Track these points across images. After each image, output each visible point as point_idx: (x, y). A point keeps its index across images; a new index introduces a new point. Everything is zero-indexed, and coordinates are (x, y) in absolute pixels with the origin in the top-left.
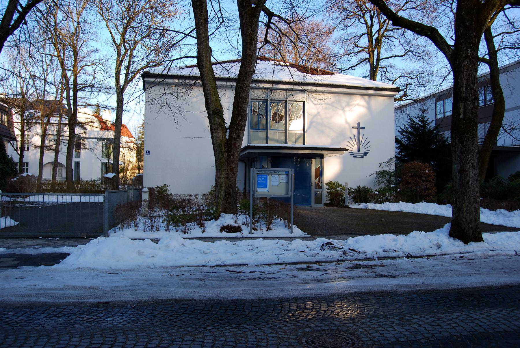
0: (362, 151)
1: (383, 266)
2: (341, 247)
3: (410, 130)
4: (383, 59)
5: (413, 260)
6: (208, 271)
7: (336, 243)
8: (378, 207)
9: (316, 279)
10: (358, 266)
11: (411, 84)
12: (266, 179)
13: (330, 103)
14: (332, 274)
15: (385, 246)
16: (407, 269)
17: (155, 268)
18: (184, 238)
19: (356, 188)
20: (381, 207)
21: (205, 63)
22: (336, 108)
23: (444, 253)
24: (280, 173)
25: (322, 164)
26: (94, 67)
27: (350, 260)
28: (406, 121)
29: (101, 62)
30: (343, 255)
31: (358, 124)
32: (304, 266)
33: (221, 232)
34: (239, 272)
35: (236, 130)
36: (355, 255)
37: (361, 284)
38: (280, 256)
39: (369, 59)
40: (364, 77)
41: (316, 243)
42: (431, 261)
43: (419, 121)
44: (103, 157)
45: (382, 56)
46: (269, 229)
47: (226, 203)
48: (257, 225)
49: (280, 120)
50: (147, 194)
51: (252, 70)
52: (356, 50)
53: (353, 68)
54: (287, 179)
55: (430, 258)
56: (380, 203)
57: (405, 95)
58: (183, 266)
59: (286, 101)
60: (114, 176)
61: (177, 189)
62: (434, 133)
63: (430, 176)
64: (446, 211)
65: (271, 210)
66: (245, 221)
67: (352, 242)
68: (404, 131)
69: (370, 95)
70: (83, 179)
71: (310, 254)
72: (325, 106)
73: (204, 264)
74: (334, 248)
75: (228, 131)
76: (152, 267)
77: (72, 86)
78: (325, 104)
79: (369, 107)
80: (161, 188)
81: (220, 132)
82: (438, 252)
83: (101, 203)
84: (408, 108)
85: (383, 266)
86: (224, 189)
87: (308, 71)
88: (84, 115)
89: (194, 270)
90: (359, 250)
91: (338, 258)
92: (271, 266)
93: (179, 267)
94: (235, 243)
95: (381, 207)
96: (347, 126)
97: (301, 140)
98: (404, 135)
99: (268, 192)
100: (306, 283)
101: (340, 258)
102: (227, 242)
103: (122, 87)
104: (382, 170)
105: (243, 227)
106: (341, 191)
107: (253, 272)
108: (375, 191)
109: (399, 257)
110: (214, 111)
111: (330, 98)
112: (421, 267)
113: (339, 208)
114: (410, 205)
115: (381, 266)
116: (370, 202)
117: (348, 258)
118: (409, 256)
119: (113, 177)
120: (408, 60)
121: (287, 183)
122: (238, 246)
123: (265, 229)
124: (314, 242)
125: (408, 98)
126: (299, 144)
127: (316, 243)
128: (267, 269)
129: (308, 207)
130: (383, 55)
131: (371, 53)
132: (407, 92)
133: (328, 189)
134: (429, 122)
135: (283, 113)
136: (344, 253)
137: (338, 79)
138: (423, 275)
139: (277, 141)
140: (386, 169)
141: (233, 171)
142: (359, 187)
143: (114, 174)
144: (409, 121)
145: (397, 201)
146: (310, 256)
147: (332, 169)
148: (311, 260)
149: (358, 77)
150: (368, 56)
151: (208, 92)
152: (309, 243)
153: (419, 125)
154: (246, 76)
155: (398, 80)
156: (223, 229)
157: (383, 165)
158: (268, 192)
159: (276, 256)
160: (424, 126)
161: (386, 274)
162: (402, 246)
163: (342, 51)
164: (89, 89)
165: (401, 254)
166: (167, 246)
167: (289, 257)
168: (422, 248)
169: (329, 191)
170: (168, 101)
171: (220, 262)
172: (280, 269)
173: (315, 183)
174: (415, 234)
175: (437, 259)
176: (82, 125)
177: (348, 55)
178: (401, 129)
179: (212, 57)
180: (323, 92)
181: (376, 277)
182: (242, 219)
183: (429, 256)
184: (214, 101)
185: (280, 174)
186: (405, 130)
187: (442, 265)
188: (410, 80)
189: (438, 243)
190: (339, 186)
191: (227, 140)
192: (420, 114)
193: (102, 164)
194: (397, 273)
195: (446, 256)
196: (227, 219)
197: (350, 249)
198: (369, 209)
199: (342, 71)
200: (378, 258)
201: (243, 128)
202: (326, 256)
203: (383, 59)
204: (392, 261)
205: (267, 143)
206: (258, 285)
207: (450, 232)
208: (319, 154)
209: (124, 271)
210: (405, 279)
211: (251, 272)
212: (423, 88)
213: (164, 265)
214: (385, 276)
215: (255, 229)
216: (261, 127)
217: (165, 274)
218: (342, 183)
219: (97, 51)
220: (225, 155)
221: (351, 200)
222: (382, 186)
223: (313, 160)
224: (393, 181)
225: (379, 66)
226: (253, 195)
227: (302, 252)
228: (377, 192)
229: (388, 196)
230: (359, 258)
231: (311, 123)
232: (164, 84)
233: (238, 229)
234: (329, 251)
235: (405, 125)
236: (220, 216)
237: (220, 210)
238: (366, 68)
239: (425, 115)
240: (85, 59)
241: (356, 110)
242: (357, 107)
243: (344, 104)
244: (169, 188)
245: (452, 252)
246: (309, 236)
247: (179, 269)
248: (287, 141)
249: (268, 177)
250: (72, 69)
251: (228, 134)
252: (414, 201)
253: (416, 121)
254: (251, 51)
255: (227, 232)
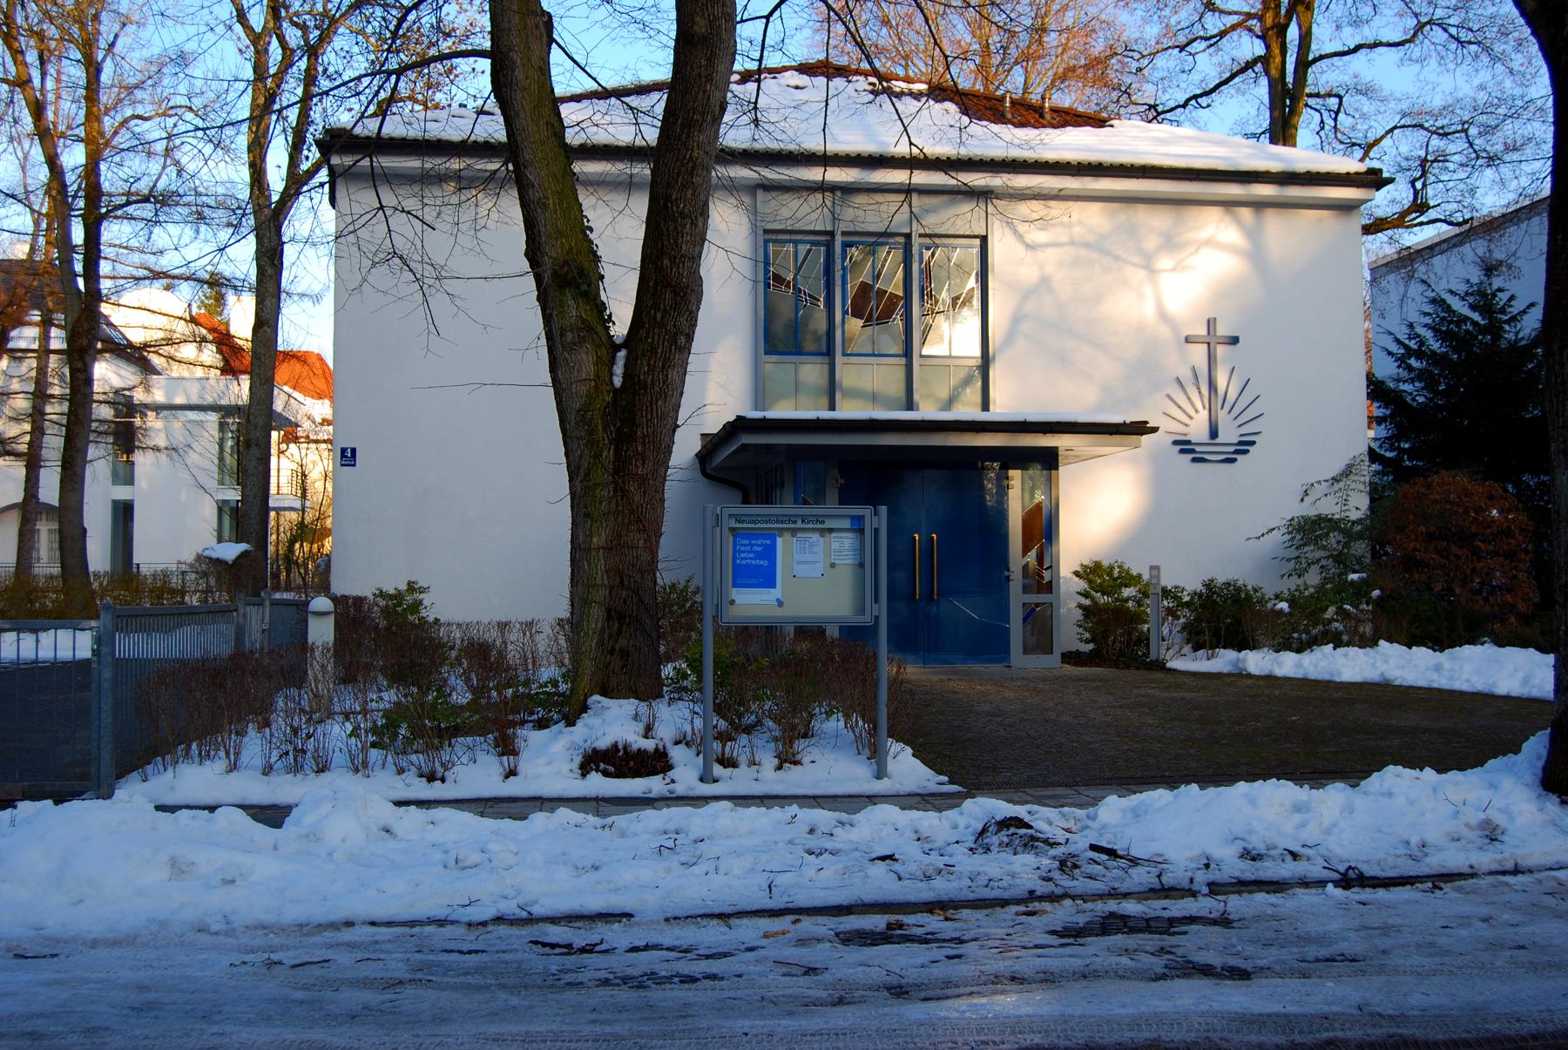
0: (1229, 434)
1: (1224, 921)
2: (1061, 837)
3: (1435, 345)
4: (1321, 58)
5: (1367, 894)
6: (452, 946)
7: (1046, 819)
8: (1287, 664)
9: (894, 980)
10: (1111, 924)
11: (1441, 158)
12: (770, 553)
13: (1090, 238)
14: (981, 960)
15: (1251, 832)
16: (1320, 940)
17: (227, 934)
18: (399, 804)
19: (1199, 587)
20: (1438, 668)
21: (519, 74)
22: (1117, 258)
23: (1509, 865)
24: (829, 524)
25: (1051, 485)
26: (170, 121)
27: (1084, 898)
28: (1416, 307)
29: (197, 103)
30: (1056, 875)
31: (1211, 324)
32: (878, 922)
33: (584, 775)
34: (583, 950)
35: (653, 349)
36: (1112, 875)
37: (1069, 1011)
38: (781, 880)
39: (1264, 60)
40: (1247, 136)
41: (962, 822)
42: (1449, 901)
43: (1473, 307)
44: (221, 482)
45: (1316, 49)
46: (787, 759)
47: (612, 652)
48: (739, 747)
49: (885, 316)
50: (329, 623)
51: (715, 102)
52: (1213, 24)
53: (1204, 101)
54: (861, 550)
55: (1447, 887)
56: (1299, 651)
57: (1419, 206)
58: (349, 924)
59: (908, 236)
60: (244, 554)
61: (455, 604)
62: (1533, 357)
63: (1507, 533)
64: (1522, 672)
65: (778, 684)
66: (688, 728)
67: (1117, 816)
68: (1409, 352)
69: (1259, 205)
70: (145, 570)
71: (912, 867)
72: (1070, 252)
73: (441, 913)
74: (1033, 842)
75: (622, 354)
76: (214, 928)
77: (81, 203)
78: (1072, 243)
79: (1256, 254)
80: (398, 597)
81: (585, 361)
82: (1486, 859)
83: (85, 663)
84: (1437, 261)
85: (1224, 921)
86: (601, 594)
87: (1003, 115)
88: (135, 313)
89: (396, 939)
90: (1135, 852)
91: (1030, 886)
92: (734, 921)
93: (334, 926)
94: (609, 820)
95: (1299, 666)
96: (1165, 332)
97: (973, 393)
98: (1410, 368)
99: (780, 603)
100: (840, 1001)
101: (1042, 888)
102: (578, 817)
103: (275, 198)
104: (1312, 512)
105: (677, 754)
106: (1139, 603)
107: (647, 948)
108: (1278, 597)
109: (1305, 883)
110: (563, 273)
111: (1092, 217)
112: (1386, 930)
113: (1123, 673)
114: (1422, 654)
115: (1214, 922)
116: (1253, 647)
117: (1079, 884)
118: (1350, 879)
119: (261, 558)
120: (1433, 62)
121: (861, 565)
122: (623, 835)
123: (769, 761)
124: (951, 814)
125: (1432, 214)
126: (967, 410)
127: (962, 822)
128: (713, 935)
129: (995, 668)
130: (1325, 38)
131: (1273, 34)
132: (1430, 191)
133: (1086, 595)
134: (1514, 311)
135: (895, 287)
136: (1063, 863)
137: (1129, 139)
138: (1382, 970)
139: (874, 398)
140: (1329, 507)
141: (639, 521)
142: (1209, 585)
143: (243, 547)
144: (1428, 309)
145: (1368, 642)
146: (912, 878)
147: (1099, 510)
148: (911, 898)
149: (1226, 132)
150: (1259, 49)
151: (533, 195)
152: (928, 820)
153: (1475, 323)
154: (690, 126)
155: (1387, 142)
156: (593, 761)
157: (1319, 490)
158: (780, 603)
159: (763, 880)
160: (1494, 329)
161: (1216, 960)
162: (1328, 832)
163: (1152, 31)
164: (146, 211)
165: (1315, 870)
166: (313, 836)
167: (820, 882)
168: (1414, 840)
169: (1087, 602)
170: (400, 243)
171: (513, 904)
172: (766, 936)
173: (1025, 567)
174: (1394, 778)
175: (1474, 892)
176: (135, 355)
177: (1182, 48)
178: (1398, 341)
179: (556, 55)
180: (1059, 196)
181: (1164, 977)
182: (673, 719)
183: (1441, 879)
184: (560, 234)
185: (831, 530)
186: (1413, 344)
187: (1485, 920)
188: (1436, 142)
189: (1487, 822)
190: (1128, 579)
191: (616, 391)
192: (1475, 280)
193: (220, 510)
194: (1268, 957)
195: (1520, 878)
196: (614, 722)
197: (1093, 847)
198: (1249, 676)
199: (1155, 113)
200: (1209, 884)
201: (682, 340)
202: (983, 880)
203: (1321, 58)
204: (1272, 898)
205: (832, 407)
206: (623, 1009)
207: (1544, 769)
208: (1035, 449)
209: (94, 944)
210: (1295, 983)
211: (635, 949)
212: (1489, 173)
213: (268, 918)
214: (1206, 971)
215: (729, 763)
216: (809, 346)
217: (247, 958)
218: (1139, 567)
219: (182, 59)
220: (608, 455)
221: (1178, 639)
222: (1313, 578)
223: (1015, 475)
224: (1359, 560)
225: (1307, 90)
226: (715, 618)
227: (883, 858)
228: (1284, 606)
229: (1331, 621)
230: (1124, 887)
231: (1016, 320)
232: (375, 179)
233: (656, 763)
234: (1007, 855)
235: (1411, 326)
236: (584, 708)
237: (585, 682)
238: (1250, 102)
239: (1497, 283)
240: (139, 94)
241: (1200, 267)
242: (1204, 251)
243: (1151, 243)
244: (427, 599)
245: (1550, 861)
246: (954, 788)
247: (329, 935)
248: (916, 397)
249: (779, 541)
250: (83, 135)
251: (619, 369)
252: (1440, 641)
253: (1458, 305)
254: (712, 23)
255: (606, 774)
